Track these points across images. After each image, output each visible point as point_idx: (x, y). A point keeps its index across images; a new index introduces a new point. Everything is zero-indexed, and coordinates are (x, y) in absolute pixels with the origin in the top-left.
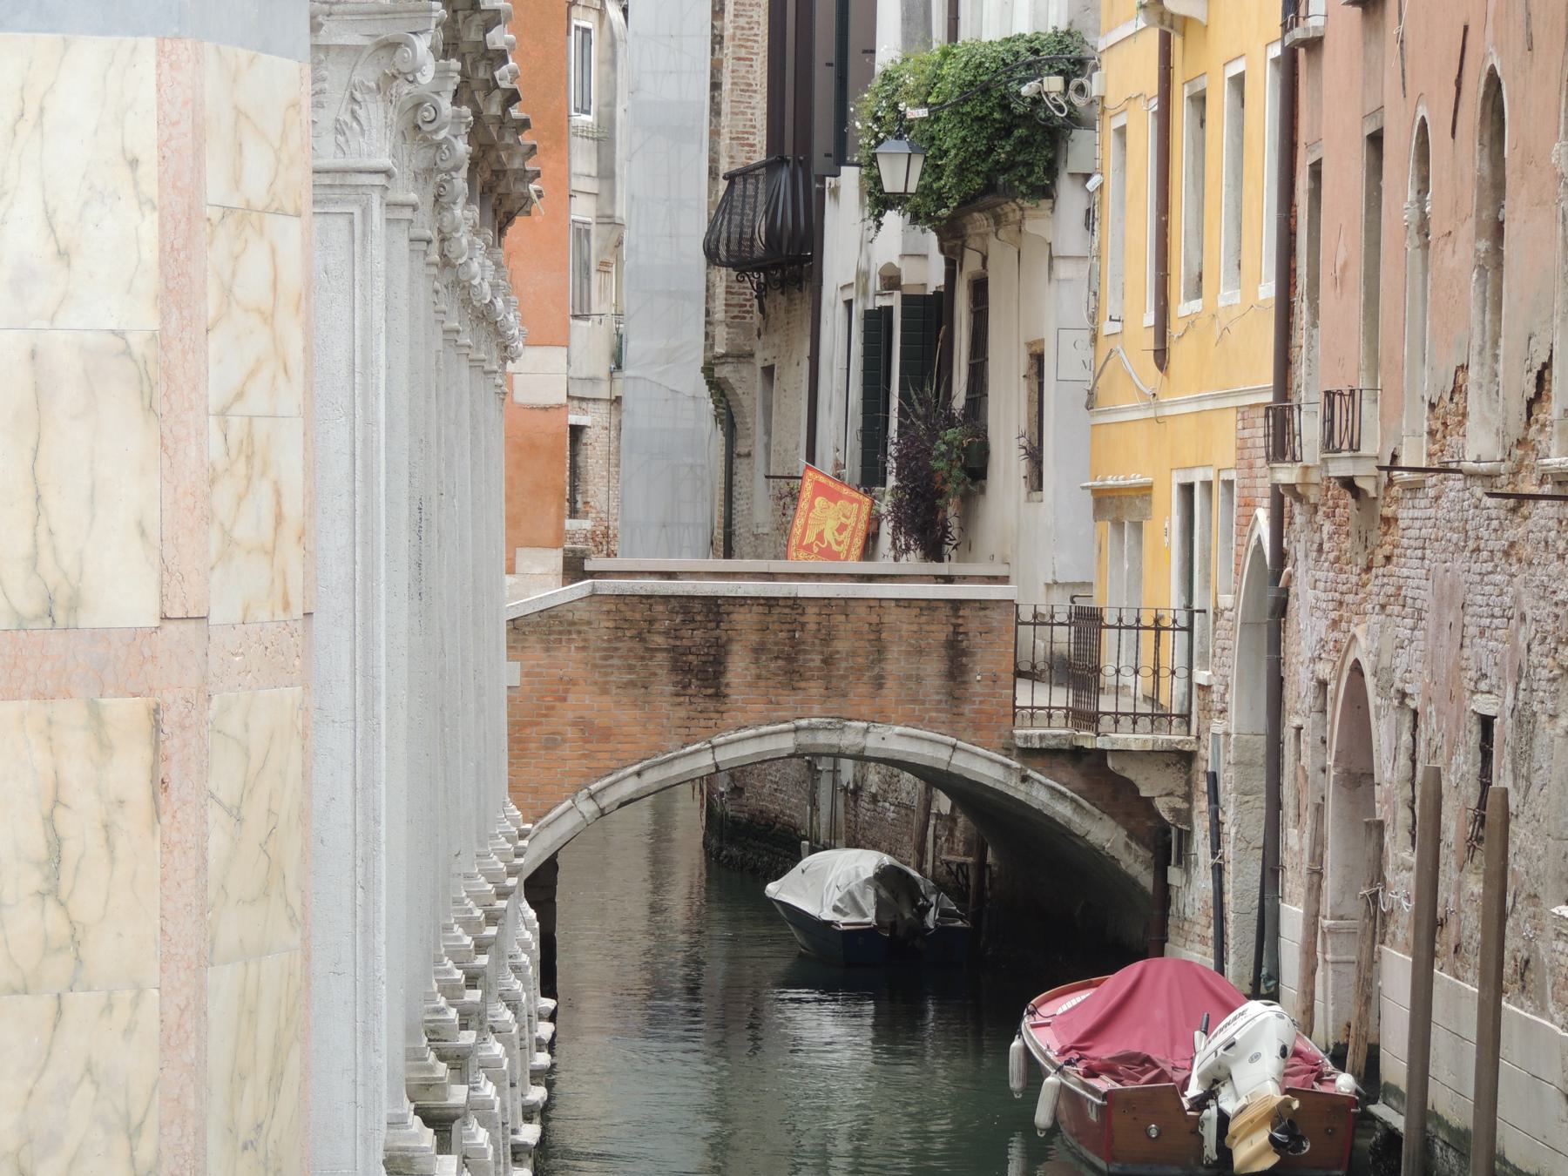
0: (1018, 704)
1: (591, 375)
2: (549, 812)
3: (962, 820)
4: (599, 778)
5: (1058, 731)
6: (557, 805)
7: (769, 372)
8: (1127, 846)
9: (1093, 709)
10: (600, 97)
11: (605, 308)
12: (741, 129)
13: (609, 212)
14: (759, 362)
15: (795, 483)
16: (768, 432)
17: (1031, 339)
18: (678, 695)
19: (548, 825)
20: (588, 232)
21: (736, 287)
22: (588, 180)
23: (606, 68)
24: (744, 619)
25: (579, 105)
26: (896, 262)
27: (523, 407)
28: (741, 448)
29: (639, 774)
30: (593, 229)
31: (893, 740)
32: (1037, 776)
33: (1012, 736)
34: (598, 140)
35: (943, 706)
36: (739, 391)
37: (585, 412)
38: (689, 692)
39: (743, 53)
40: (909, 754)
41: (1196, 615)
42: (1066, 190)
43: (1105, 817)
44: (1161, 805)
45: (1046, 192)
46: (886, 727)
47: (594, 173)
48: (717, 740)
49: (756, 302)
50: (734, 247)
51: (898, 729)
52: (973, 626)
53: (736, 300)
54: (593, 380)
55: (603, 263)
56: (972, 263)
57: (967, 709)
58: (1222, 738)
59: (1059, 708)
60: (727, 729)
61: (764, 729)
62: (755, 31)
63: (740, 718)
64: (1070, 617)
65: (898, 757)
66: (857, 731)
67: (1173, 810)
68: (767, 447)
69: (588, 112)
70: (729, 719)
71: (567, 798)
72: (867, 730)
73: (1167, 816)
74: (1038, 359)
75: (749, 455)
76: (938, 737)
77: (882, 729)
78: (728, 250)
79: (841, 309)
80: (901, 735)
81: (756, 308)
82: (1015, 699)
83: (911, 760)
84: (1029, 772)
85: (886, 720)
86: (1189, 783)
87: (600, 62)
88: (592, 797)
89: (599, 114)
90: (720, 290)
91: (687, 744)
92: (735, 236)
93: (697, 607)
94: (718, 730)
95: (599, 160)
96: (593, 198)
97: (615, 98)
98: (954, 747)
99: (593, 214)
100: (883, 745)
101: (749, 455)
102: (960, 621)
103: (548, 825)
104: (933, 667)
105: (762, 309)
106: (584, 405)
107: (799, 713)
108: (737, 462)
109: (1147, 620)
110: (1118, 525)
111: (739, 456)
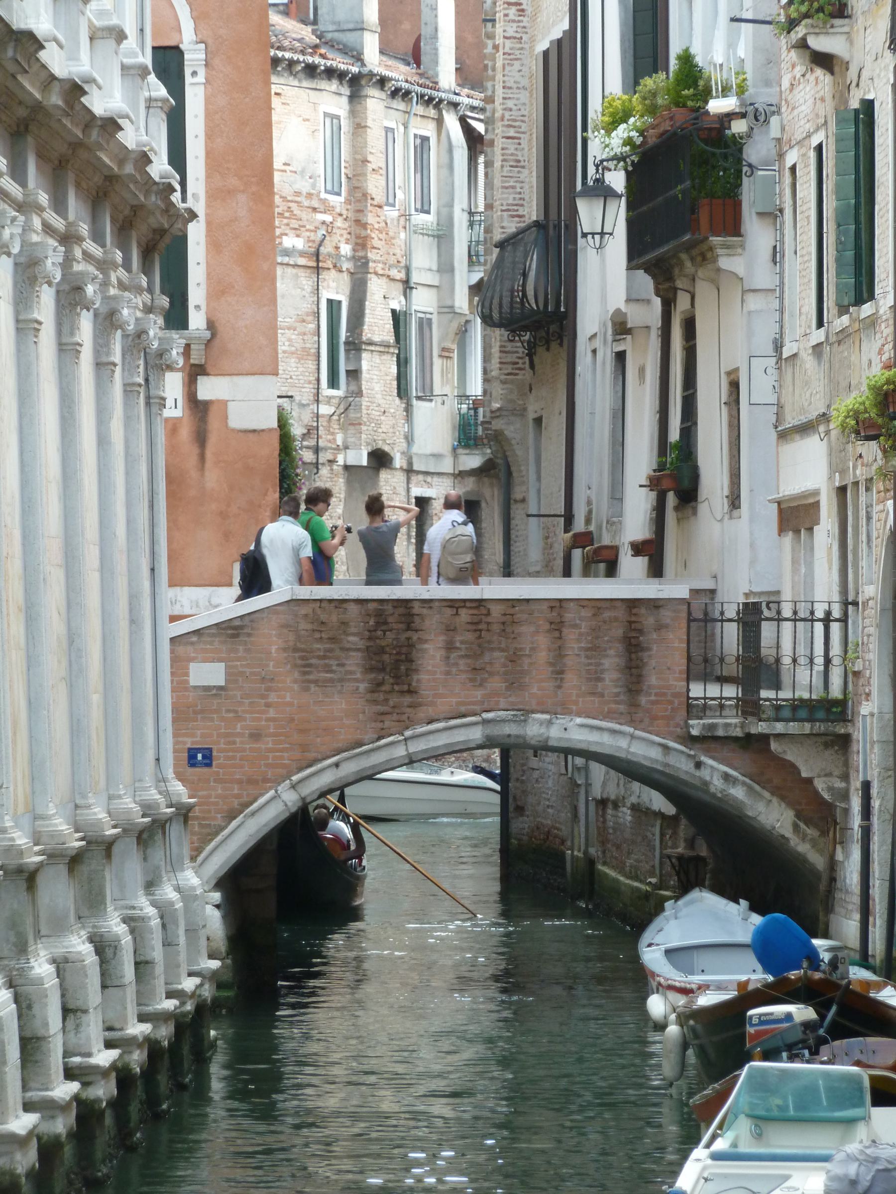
0: (691, 695)
1: (435, 451)
2: (255, 800)
3: (684, 821)
4: (300, 769)
5: (731, 723)
6: (262, 795)
7: (538, 421)
8: (796, 827)
9: (755, 698)
10: (439, 199)
11: (447, 390)
12: (511, 201)
13: (449, 303)
14: (531, 415)
15: (78, 348)
16: (539, 479)
17: (728, 369)
18: (373, 692)
19: (253, 814)
20: (430, 321)
21: (509, 347)
22: (429, 274)
23: (445, 172)
24: (432, 622)
25: (419, 206)
26: (623, 308)
27: (233, 430)
28: (517, 494)
29: (337, 765)
30: (435, 318)
31: (574, 730)
32: (710, 762)
33: (687, 726)
34: (439, 237)
35: (622, 697)
36: (513, 442)
37: (430, 485)
38: (383, 688)
39: (512, 133)
40: (589, 743)
41: (850, 607)
42: (752, 225)
43: (775, 800)
44: (820, 785)
45: (732, 226)
46: (568, 718)
47: (435, 267)
48: (408, 733)
49: (527, 359)
50: (506, 309)
51: (579, 720)
52: (649, 621)
53: (510, 358)
54: (437, 456)
55: (444, 349)
56: (682, 303)
57: (643, 700)
58: (868, 719)
59: (730, 699)
60: (420, 723)
61: (453, 722)
62: (523, 112)
63: (431, 711)
64: (738, 613)
65: (583, 746)
66: (541, 723)
67: (830, 789)
68: (539, 491)
69: (428, 212)
70: (422, 714)
71: (270, 788)
72: (550, 723)
73: (826, 796)
74: (735, 386)
75: (523, 500)
76: (617, 727)
77: (562, 721)
78: (500, 313)
79: (589, 354)
80: (582, 726)
81: (527, 365)
82: (688, 690)
83: (593, 748)
84: (703, 758)
85: (567, 712)
86: (846, 764)
87: (439, 167)
88: (293, 787)
89: (438, 214)
90: (495, 350)
91: (379, 738)
92: (506, 301)
93: (389, 608)
94: (410, 723)
95: (439, 256)
96: (434, 291)
97: (453, 199)
98: (632, 737)
99: (435, 304)
100: (566, 735)
101: (523, 500)
102: (633, 619)
103: (253, 814)
104: (612, 662)
105: (532, 366)
106: (429, 479)
107: (486, 706)
108: (514, 507)
109: (820, 614)
110: (797, 532)
111: (516, 501)
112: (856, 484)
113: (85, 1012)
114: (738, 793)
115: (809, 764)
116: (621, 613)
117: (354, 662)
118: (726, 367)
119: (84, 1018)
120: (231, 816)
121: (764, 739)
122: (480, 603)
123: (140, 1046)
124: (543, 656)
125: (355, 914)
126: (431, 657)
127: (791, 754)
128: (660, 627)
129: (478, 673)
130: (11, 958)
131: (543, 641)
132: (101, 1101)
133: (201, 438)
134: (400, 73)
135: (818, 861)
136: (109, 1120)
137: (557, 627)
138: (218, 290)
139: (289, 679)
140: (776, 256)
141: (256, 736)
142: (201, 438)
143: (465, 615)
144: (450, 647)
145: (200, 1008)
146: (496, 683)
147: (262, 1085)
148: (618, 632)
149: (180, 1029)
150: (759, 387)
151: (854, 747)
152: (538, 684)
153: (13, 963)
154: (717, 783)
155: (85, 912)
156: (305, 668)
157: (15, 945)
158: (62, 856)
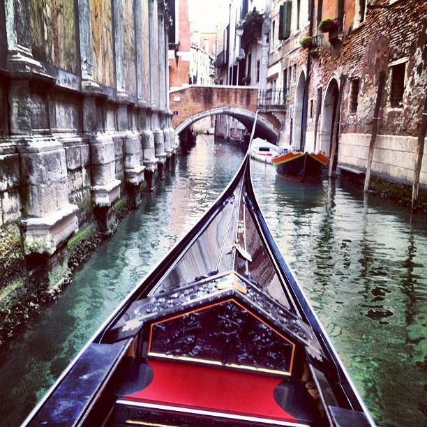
44: (280, 120)
52: (251, 92)
56: (249, 53)
74: (259, 63)
104: (244, 100)
110: (272, 82)
112: (290, 68)
113: (132, 155)
114: (264, 122)
115: (278, 117)
116: (246, 91)
117: (202, 98)
118: (258, 59)
119: (132, 157)
120: (181, 123)
121: (271, 112)
122: (223, 88)
123: (155, 164)
124: (233, 98)
125: (195, 144)
126: (215, 97)
127: (276, 115)
128: (253, 93)
129: (222, 101)
130: (89, 132)
131: (233, 95)
132: (136, 183)
133: (177, 62)
134: (202, 50)
135: (277, 134)
136: (164, 166)
137: (236, 93)
138: (180, 37)
139: (191, 100)
140: (268, 41)
141: (185, 110)
142: (177, 62)
143: (221, 90)
144: (218, 96)
145: (173, 155)
146: (226, 102)
147: (184, 167)
148: (246, 94)
149: (168, 159)
150: (264, 62)
151: (287, 116)
152: (232, 102)
153: (90, 134)
154: (261, 121)
155: (140, 128)
156: (194, 98)
157: (91, 127)
158: (125, 104)
